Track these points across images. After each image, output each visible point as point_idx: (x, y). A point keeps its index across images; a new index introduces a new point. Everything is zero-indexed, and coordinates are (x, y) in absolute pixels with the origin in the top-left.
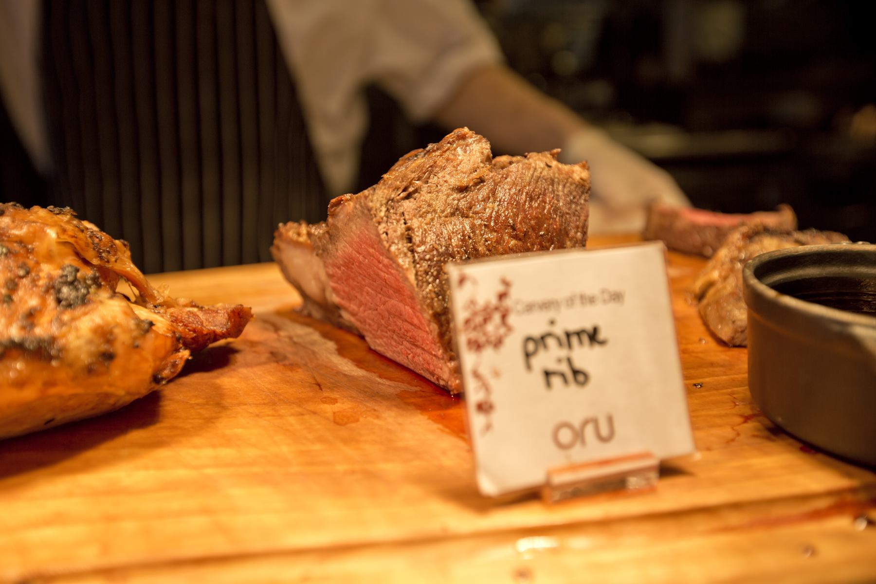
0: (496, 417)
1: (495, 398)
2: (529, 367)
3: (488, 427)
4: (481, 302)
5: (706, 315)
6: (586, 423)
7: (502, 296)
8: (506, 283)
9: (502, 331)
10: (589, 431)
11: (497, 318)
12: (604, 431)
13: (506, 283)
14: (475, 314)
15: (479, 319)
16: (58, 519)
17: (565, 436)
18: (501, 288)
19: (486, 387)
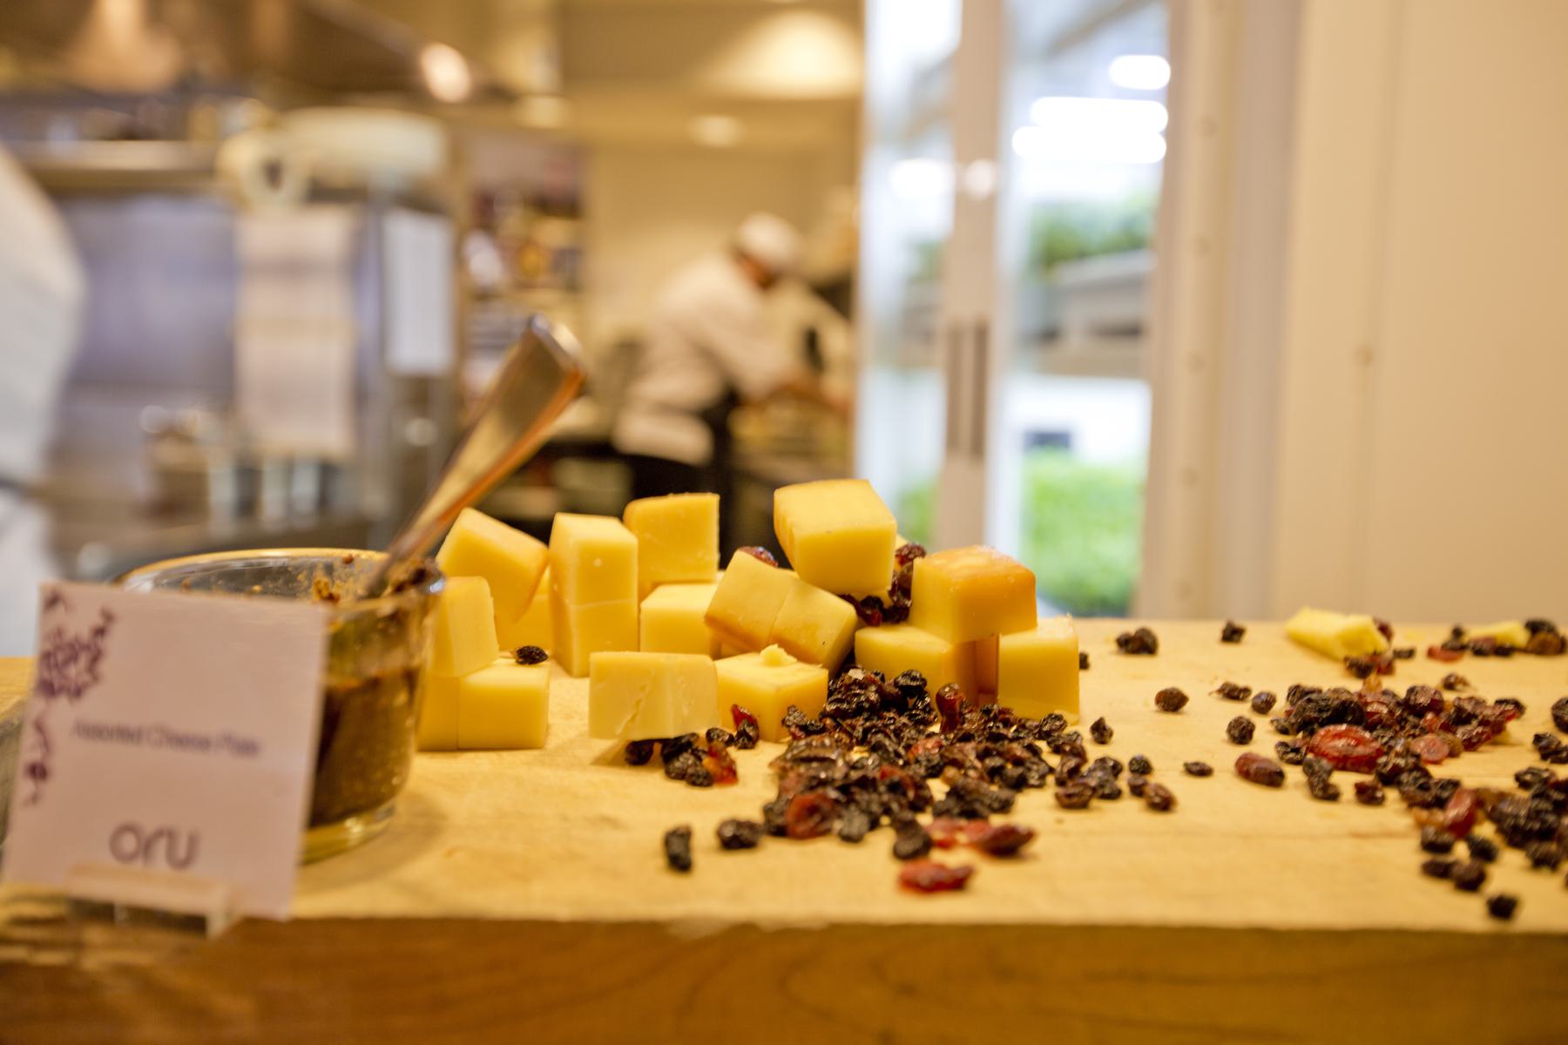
0: (50, 788)
1: (57, 764)
2: (1164, 804)
3: (35, 799)
4: (70, 634)
5: (952, 440)
6: (159, 834)
7: (100, 632)
8: (108, 617)
9: (86, 678)
10: (161, 847)
11: (83, 660)
12: (182, 852)
13: (108, 617)
14: (58, 648)
15: (60, 657)
16: (1339, 736)
17: (129, 843)
18: (98, 621)
19: (46, 745)
